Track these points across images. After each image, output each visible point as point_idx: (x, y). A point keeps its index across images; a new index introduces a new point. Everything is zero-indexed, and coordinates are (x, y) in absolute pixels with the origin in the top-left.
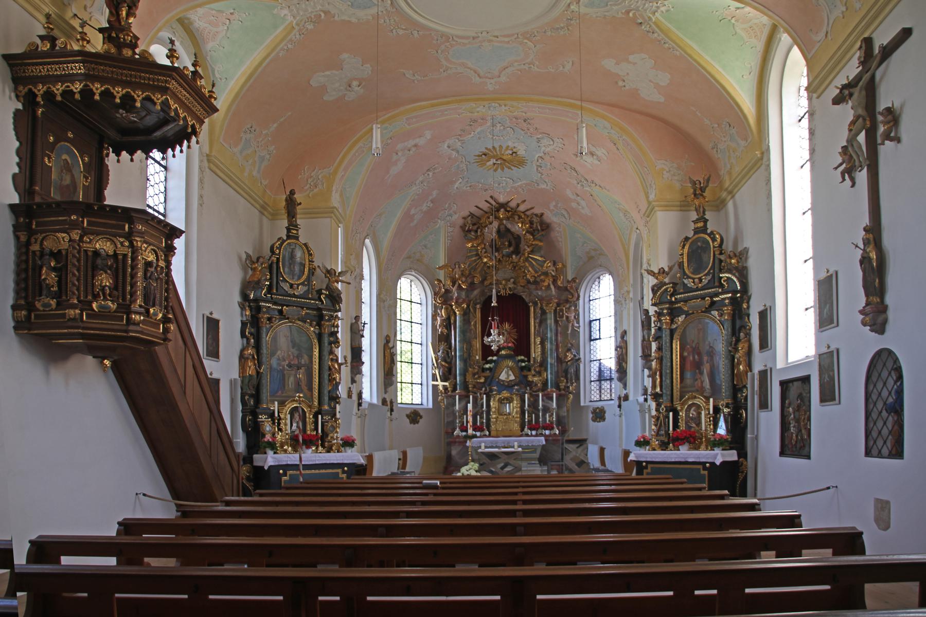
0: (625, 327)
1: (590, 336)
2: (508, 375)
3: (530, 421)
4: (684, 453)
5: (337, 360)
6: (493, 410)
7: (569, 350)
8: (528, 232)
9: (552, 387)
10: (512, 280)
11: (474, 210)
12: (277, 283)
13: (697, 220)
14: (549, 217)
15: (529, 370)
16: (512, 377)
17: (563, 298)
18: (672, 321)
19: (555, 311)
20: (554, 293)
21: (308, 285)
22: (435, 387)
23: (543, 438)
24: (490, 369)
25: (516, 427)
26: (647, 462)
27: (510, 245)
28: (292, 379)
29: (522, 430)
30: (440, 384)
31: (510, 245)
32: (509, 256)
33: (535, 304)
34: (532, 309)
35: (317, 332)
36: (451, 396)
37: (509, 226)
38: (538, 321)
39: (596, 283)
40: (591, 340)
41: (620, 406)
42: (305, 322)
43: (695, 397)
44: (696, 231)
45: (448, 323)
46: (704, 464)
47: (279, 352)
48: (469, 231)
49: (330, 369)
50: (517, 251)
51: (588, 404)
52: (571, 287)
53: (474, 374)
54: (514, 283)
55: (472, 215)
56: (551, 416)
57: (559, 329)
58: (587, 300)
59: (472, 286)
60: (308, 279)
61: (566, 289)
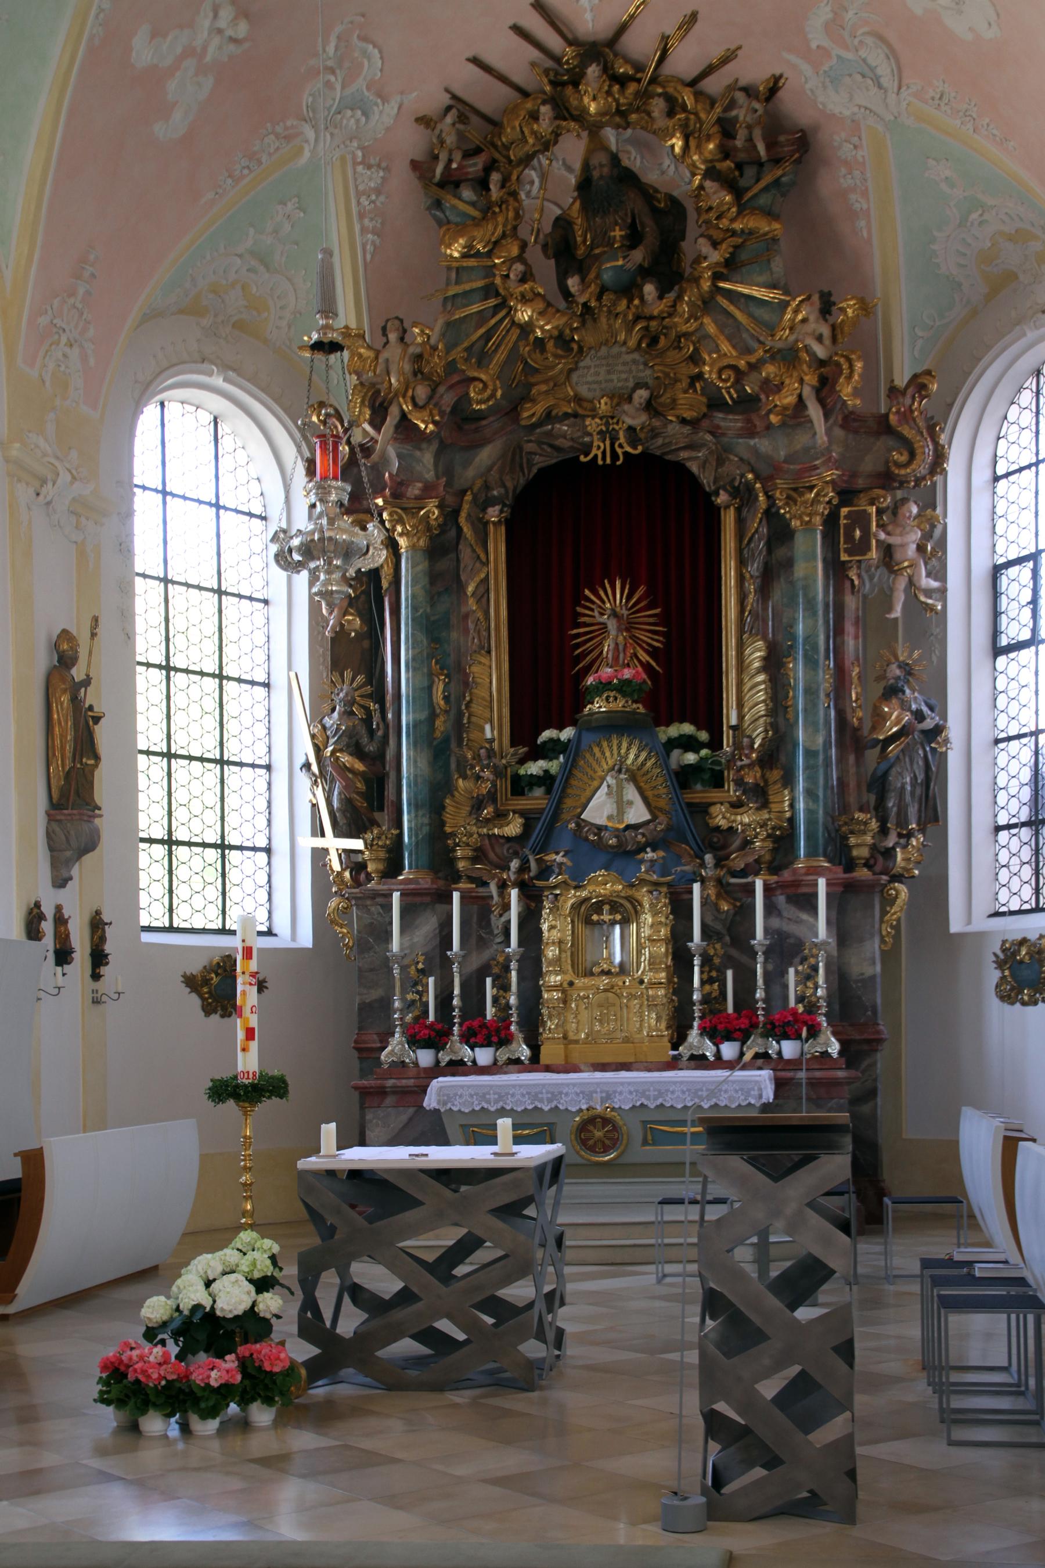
1: (996, 633)
2: (621, 805)
3: (713, 1002)
6: (551, 952)
7: (892, 692)
8: (711, 173)
9: (811, 853)
10: (641, 395)
11: (468, 81)
14: (818, 95)
15: (717, 781)
16: (638, 813)
17: (869, 464)
19: (831, 521)
22: (319, 855)
23: (764, 1077)
24: (546, 780)
25: (651, 1024)
27: (634, 239)
29: (679, 1039)
30: (335, 844)
32: (629, 289)
33: (743, 495)
34: (729, 519)
36: (375, 895)
37: (633, 160)
38: (754, 569)
39: (1026, 397)
40: (997, 651)
45: (370, 594)
48: (451, 183)
50: (667, 270)
51: (981, 923)
52: (907, 416)
53: (478, 805)
55: (460, 107)
56: (810, 975)
57: (851, 602)
58: (981, 475)
59: (462, 421)
61: (884, 427)
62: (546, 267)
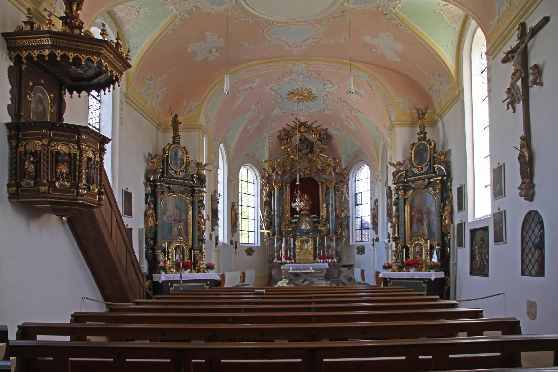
0: (377, 197)
1: (356, 202)
2: (306, 226)
3: (319, 254)
4: (412, 273)
5: (203, 217)
6: (297, 247)
7: (343, 211)
8: (318, 140)
9: (332, 233)
10: (309, 169)
11: (285, 127)
12: (167, 170)
13: (420, 132)
14: (331, 131)
15: (319, 223)
16: (309, 228)
17: (339, 179)
18: (405, 194)
19: (335, 187)
20: (334, 176)
21: (186, 172)
23: (327, 264)
24: (295, 222)
25: (311, 257)
26: (390, 279)
27: (307, 148)
28: (176, 228)
29: (315, 259)
30: (265, 231)
31: (307, 148)
32: (307, 154)
33: (323, 183)
34: (321, 186)
35: (191, 200)
36: (272, 239)
37: (307, 136)
38: (324, 193)
39: (359, 171)
40: (356, 205)
41: (373, 245)
42: (184, 194)
43: (419, 240)
44: (420, 139)
45: (270, 195)
46: (424, 279)
47: (168, 212)
48: (283, 139)
49: (199, 223)
50: (312, 152)
51: (354, 243)
52: (344, 173)
53: (286, 226)
54: (310, 171)
55: (284, 130)
56: (332, 251)
57: (337, 198)
58: (354, 181)
59: (284, 172)
60: (186, 168)
61: (341, 174)
62: (295, 150)
